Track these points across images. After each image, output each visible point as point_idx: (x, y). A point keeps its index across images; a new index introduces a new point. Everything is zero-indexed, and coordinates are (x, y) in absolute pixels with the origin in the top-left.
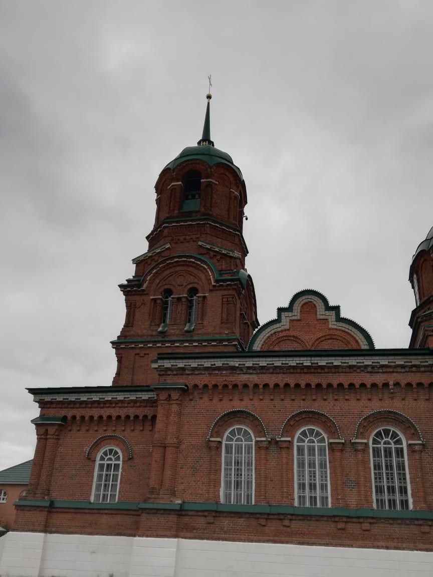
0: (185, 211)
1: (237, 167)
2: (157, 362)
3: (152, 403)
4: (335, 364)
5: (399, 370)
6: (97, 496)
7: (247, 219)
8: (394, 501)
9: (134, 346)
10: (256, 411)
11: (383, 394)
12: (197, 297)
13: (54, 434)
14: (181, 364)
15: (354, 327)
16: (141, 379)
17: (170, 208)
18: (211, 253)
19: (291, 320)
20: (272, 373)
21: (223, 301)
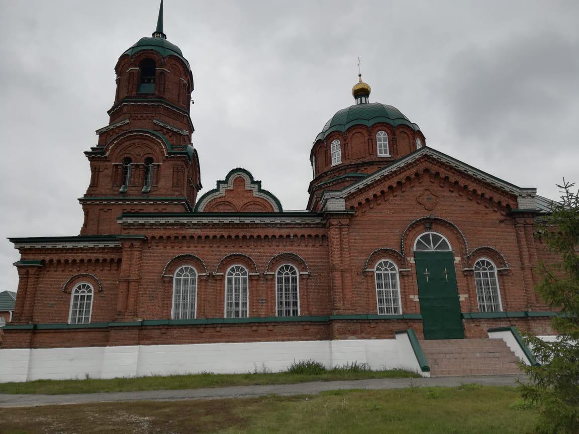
1: (186, 60)
3: (117, 250)
4: (256, 222)
6: (74, 319)
7: (193, 103)
8: (289, 311)
9: (98, 203)
16: (105, 230)
17: (128, 89)
18: (164, 130)
19: (226, 190)
20: (212, 228)
21: (174, 170)
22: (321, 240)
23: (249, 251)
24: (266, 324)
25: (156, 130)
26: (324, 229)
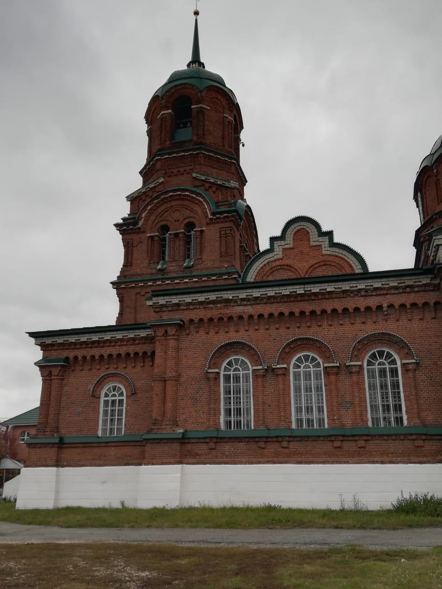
0: (177, 141)
2: (152, 300)
3: (150, 340)
4: (328, 290)
5: (393, 291)
6: (104, 430)
7: (243, 145)
9: (134, 285)
10: (252, 341)
11: (377, 316)
12: (195, 231)
13: (58, 375)
14: (175, 300)
15: (348, 252)
19: (284, 249)
20: (266, 303)
21: (220, 234)
22: (433, 309)
23: (323, 332)
24: (354, 437)
25: (196, 187)
26: (436, 293)
